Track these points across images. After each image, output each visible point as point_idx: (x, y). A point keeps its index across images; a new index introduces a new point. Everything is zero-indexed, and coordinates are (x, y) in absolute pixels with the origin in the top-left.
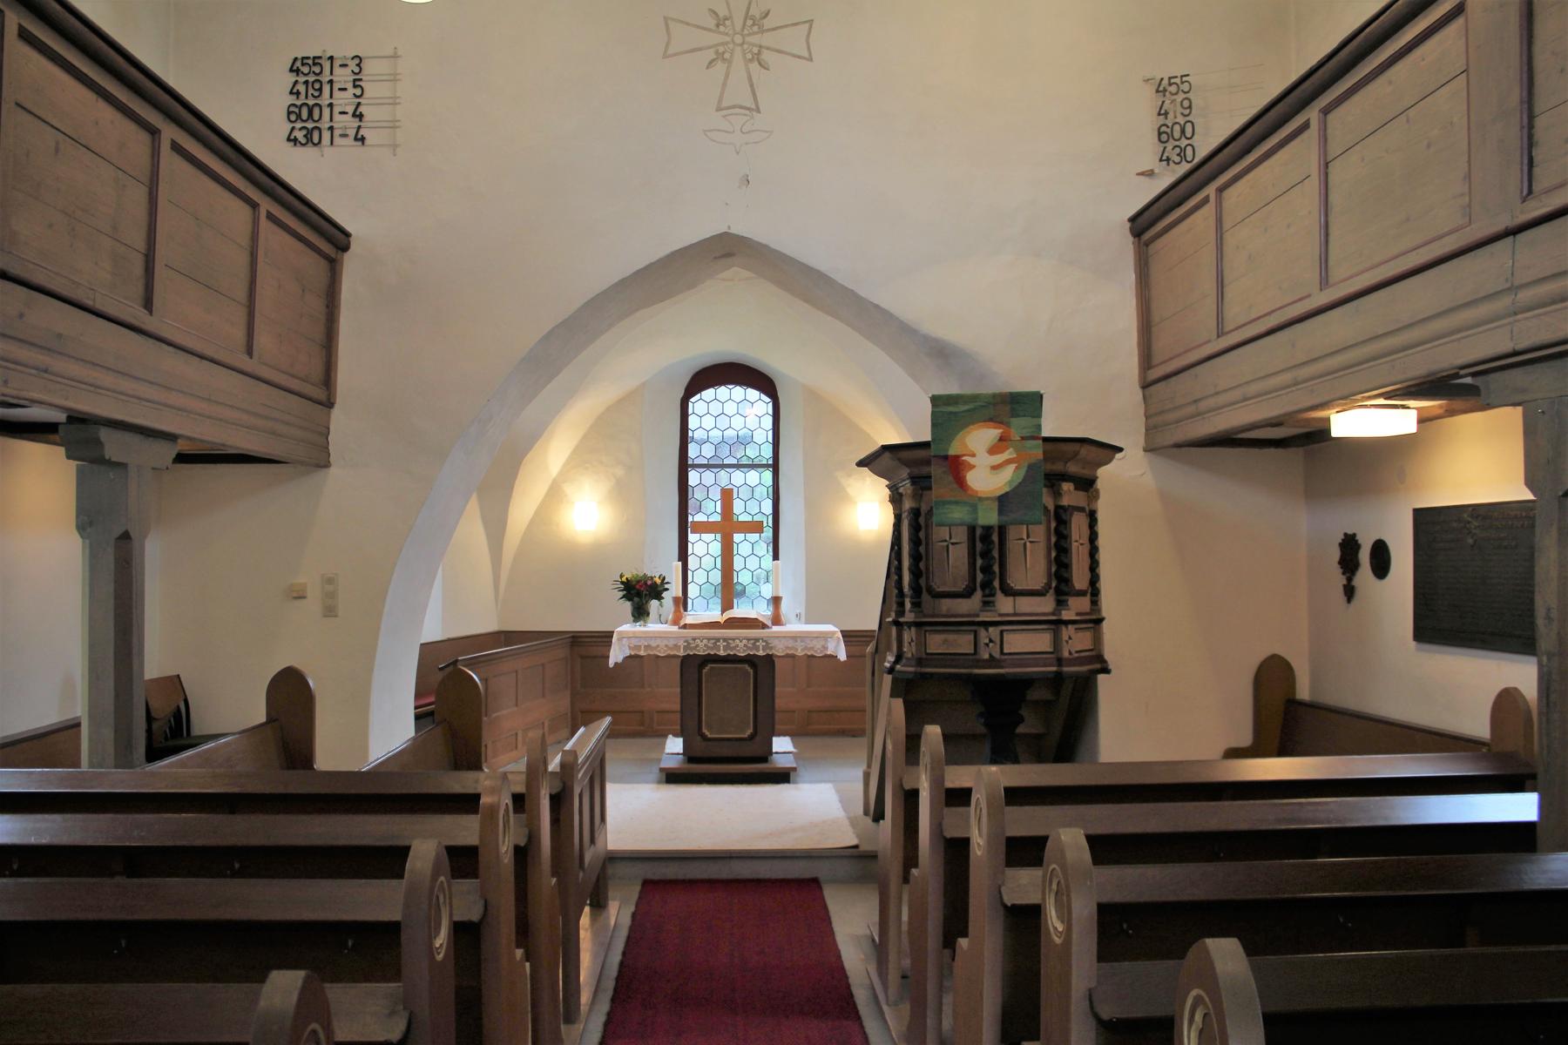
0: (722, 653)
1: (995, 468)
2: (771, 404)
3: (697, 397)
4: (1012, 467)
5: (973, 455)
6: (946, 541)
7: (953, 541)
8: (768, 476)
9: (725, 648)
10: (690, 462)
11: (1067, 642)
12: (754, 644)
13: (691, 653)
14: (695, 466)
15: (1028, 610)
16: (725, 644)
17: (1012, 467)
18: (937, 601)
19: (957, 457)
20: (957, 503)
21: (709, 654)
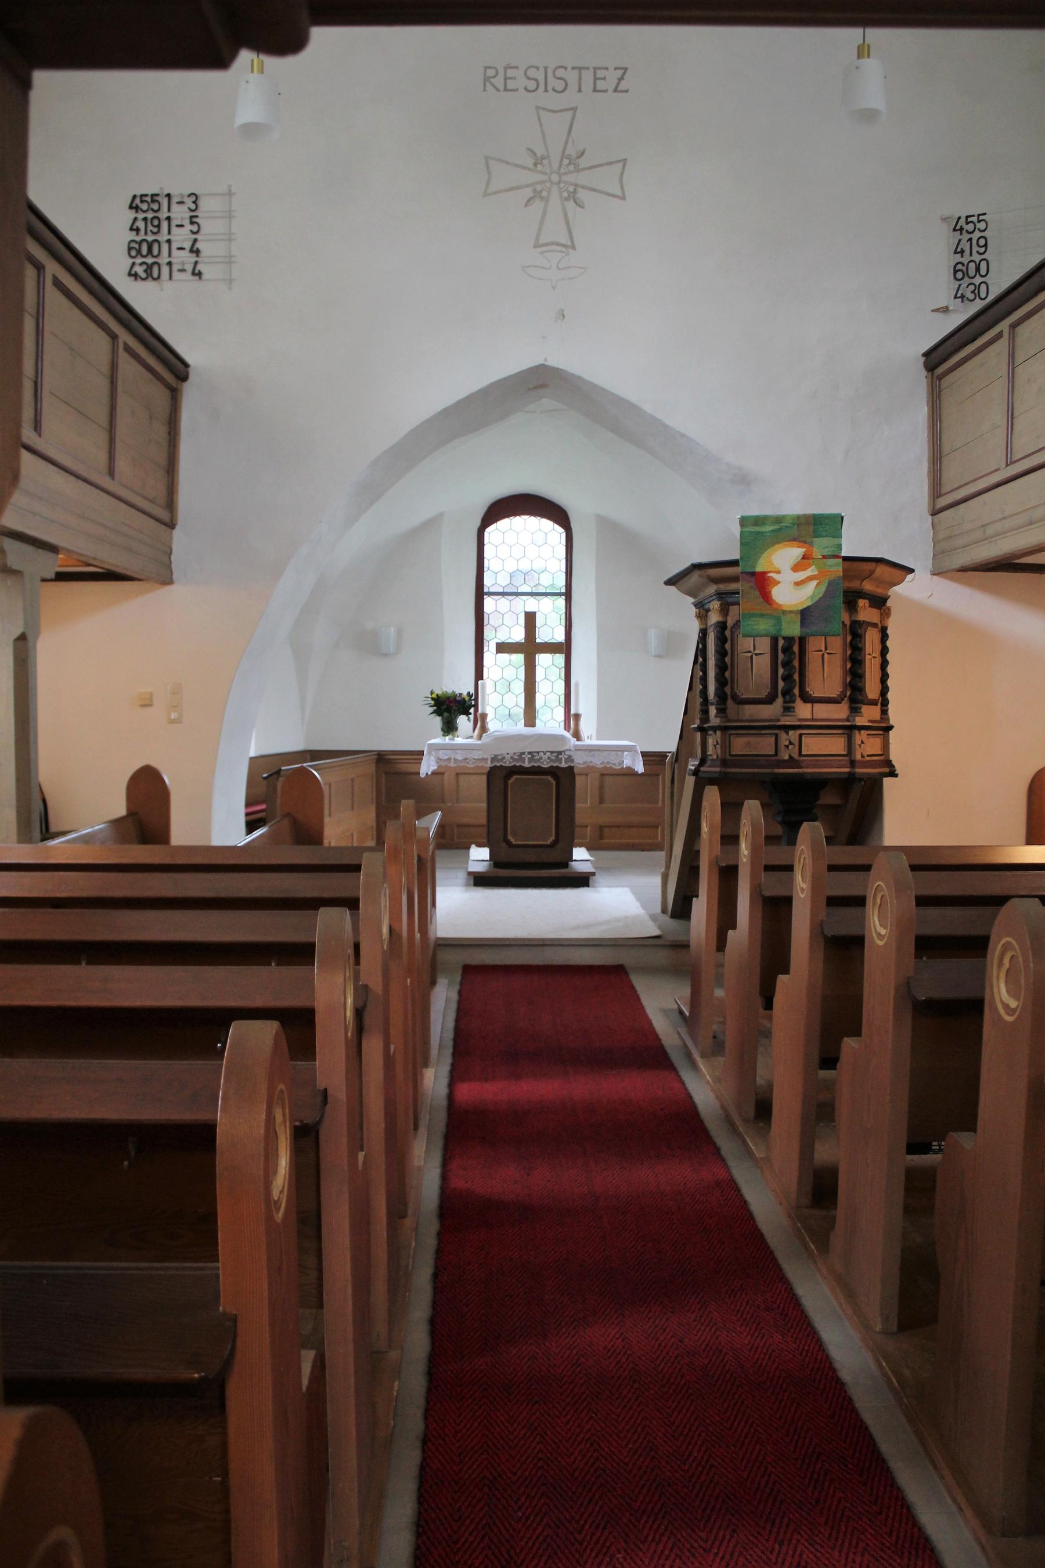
0: (527, 765)
1: (798, 584)
2: (564, 535)
3: (494, 526)
4: (814, 583)
5: (779, 572)
6: (750, 652)
7: (756, 652)
8: (561, 601)
9: (531, 760)
10: (486, 590)
11: (860, 746)
12: (557, 757)
13: (498, 765)
14: (490, 594)
15: (747, 716)
16: (530, 756)
17: (814, 583)
18: (741, 706)
19: (765, 573)
20: (762, 616)
21: (515, 766)
